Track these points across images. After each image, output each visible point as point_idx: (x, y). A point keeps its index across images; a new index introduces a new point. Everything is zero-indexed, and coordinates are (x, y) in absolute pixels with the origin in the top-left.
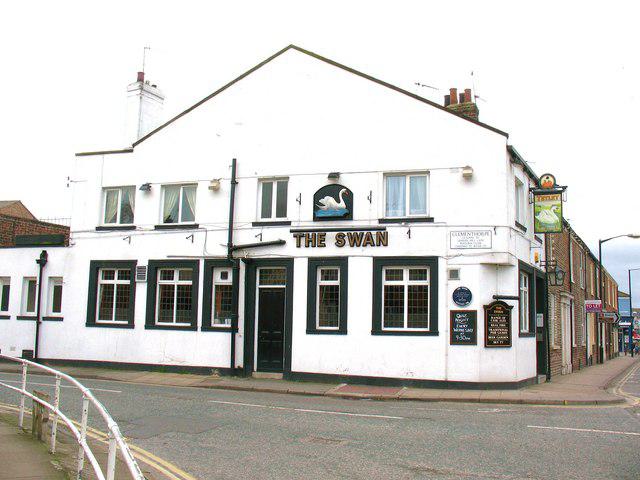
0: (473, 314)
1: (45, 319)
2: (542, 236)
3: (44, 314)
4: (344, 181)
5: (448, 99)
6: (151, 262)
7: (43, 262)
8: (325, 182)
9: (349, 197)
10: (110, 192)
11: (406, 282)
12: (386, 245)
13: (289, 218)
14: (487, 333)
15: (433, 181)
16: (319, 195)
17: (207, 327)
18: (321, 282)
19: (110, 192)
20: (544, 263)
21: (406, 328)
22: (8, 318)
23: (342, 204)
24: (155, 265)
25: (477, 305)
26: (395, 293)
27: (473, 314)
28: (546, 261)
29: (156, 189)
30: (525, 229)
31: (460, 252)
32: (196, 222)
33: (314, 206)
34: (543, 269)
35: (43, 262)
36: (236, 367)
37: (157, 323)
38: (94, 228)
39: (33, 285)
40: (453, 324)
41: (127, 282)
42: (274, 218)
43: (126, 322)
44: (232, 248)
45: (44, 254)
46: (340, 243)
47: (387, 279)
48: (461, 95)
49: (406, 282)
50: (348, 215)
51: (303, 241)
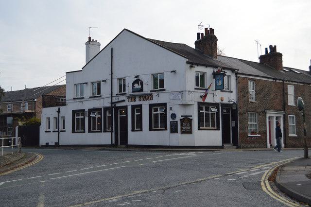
1: (61, 131)
4: (140, 78)
7: (59, 112)
9: (142, 83)
14: (182, 129)
16: (134, 84)
17: (105, 131)
18: (136, 114)
21: (159, 128)
23: (140, 86)
27: (177, 122)
29: (89, 84)
35: (59, 112)
41: (139, 114)
44: (112, 103)
47: (136, 112)
49: (159, 112)
50: (141, 90)
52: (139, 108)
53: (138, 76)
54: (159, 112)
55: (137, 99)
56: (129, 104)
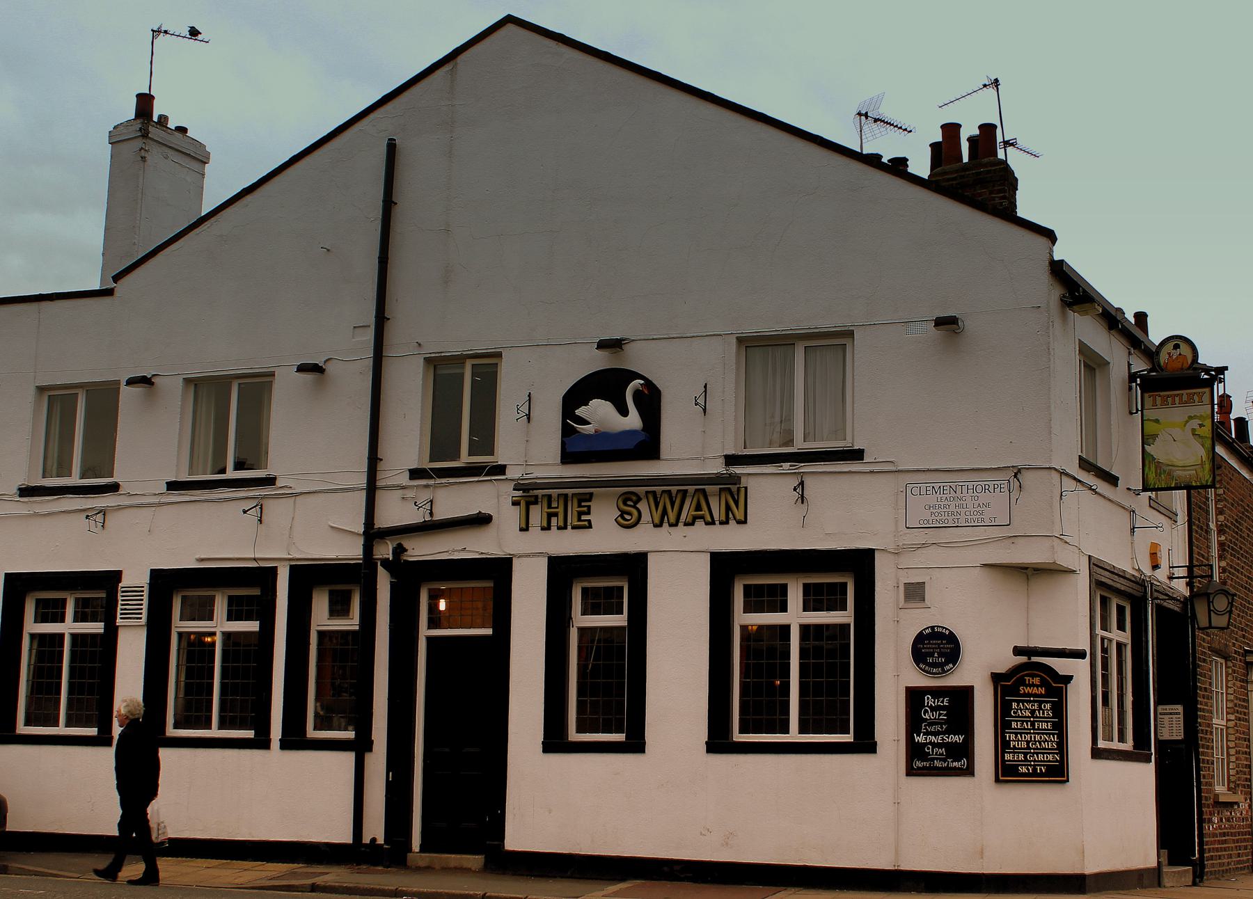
0: (963, 697)
2: (1178, 500)
5: (944, 150)
8: (596, 361)
9: (650, 402)
10: (433, 363)
11: (795, 616)
12: (744, 522)
13: (501, 456)
14: (1002, 745)
15: (862, 351)
16: (576, 396)
17: (295, 740)
18: (581, 620)
19: (433, 363)
20: (1182, 572)
21: (794, 735)
23: (633, 420)
27: (963, 697)
28: (1190, 568)
29: (172, 387)
30: (1112, 480)
31: (932, 536)
33: (565, 425)
34: (1181, 587)
36: (366, 839)
37: (312, 733)
38: (15, 490)
40: (914, 722)
41: (97, 627)
42: (465, 459)
43: (249, 734)
44: (372, 535)
46: (628, 521)
47: (747, 609)
48: (970, 140)
49: (795, 616)
51: (537, 514)
52: (256, 592)
53: (612, 345)
54: (220, 625)
55: (604, 514)
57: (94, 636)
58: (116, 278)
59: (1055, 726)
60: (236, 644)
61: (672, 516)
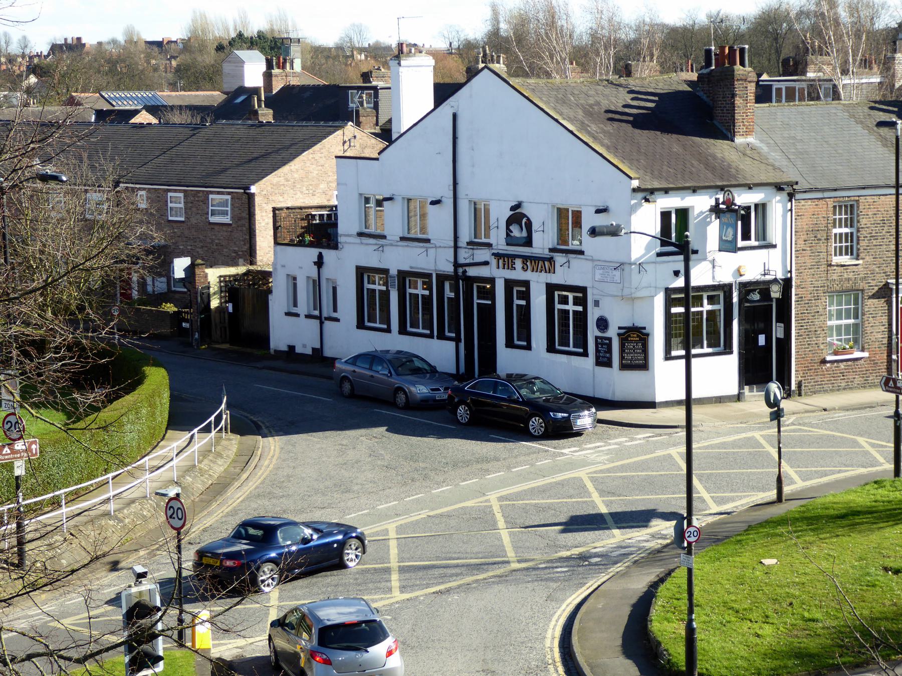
1: (327, 319)
3: (325, 314)
6: (399, 272)
7: (319, 263)
9: (529, 225)
14: (622, 358)
21: (571, 349)
22: (297, 315)
24: (403, 275)
25: (612, 332)
26: (565, 327)
27: (610, 339)
32: (429, 237)
35: (319, 263)
39: (316, 285)
44: (456, 265)
45: (320, 256)
46: (525, 269)
50: (528, 242)
55: (518, 263)
56: (500, 275)
57: (675, 306)
58: (379, 154)
59: (643, 351)
60: (425, 298)
61: (535, 269)
